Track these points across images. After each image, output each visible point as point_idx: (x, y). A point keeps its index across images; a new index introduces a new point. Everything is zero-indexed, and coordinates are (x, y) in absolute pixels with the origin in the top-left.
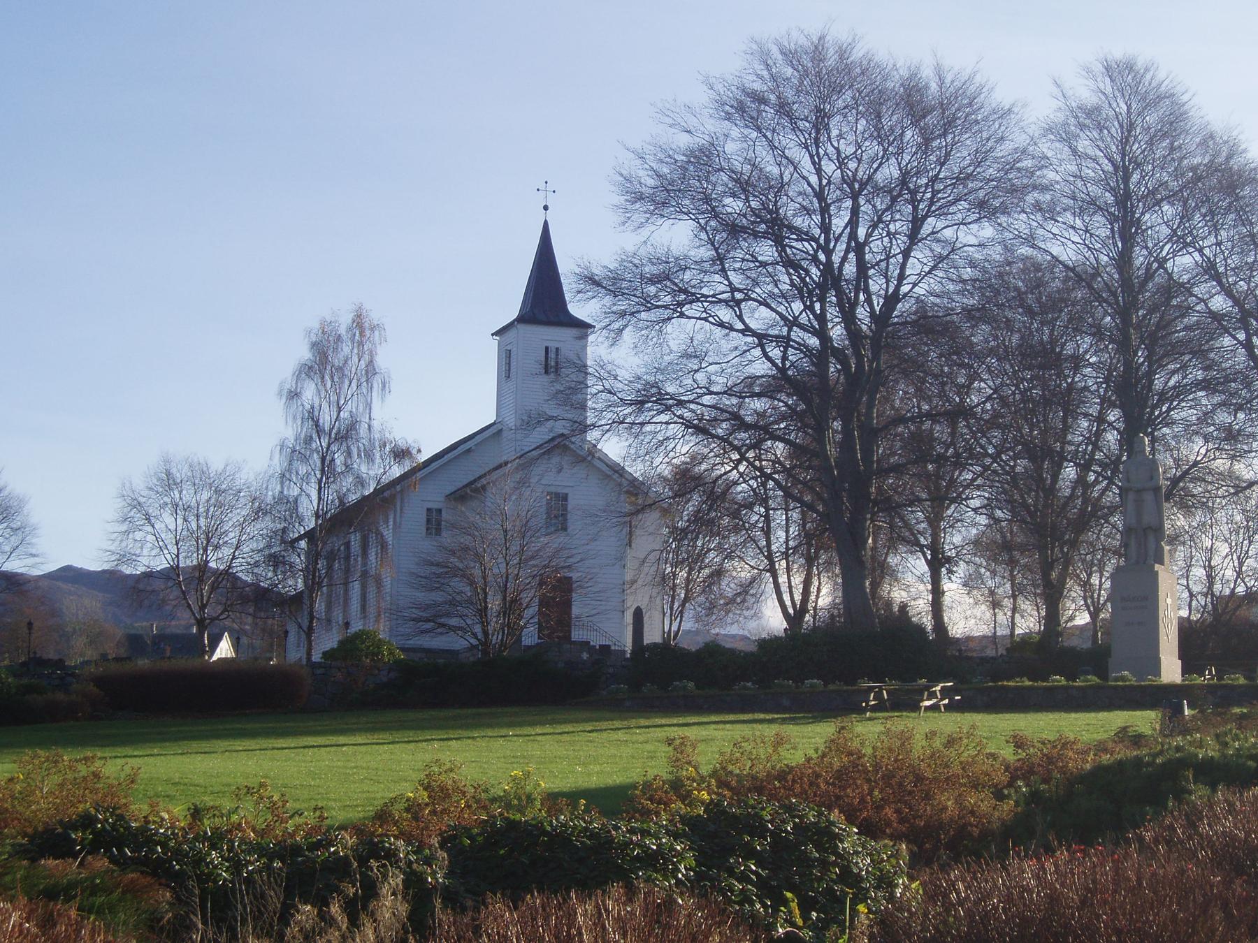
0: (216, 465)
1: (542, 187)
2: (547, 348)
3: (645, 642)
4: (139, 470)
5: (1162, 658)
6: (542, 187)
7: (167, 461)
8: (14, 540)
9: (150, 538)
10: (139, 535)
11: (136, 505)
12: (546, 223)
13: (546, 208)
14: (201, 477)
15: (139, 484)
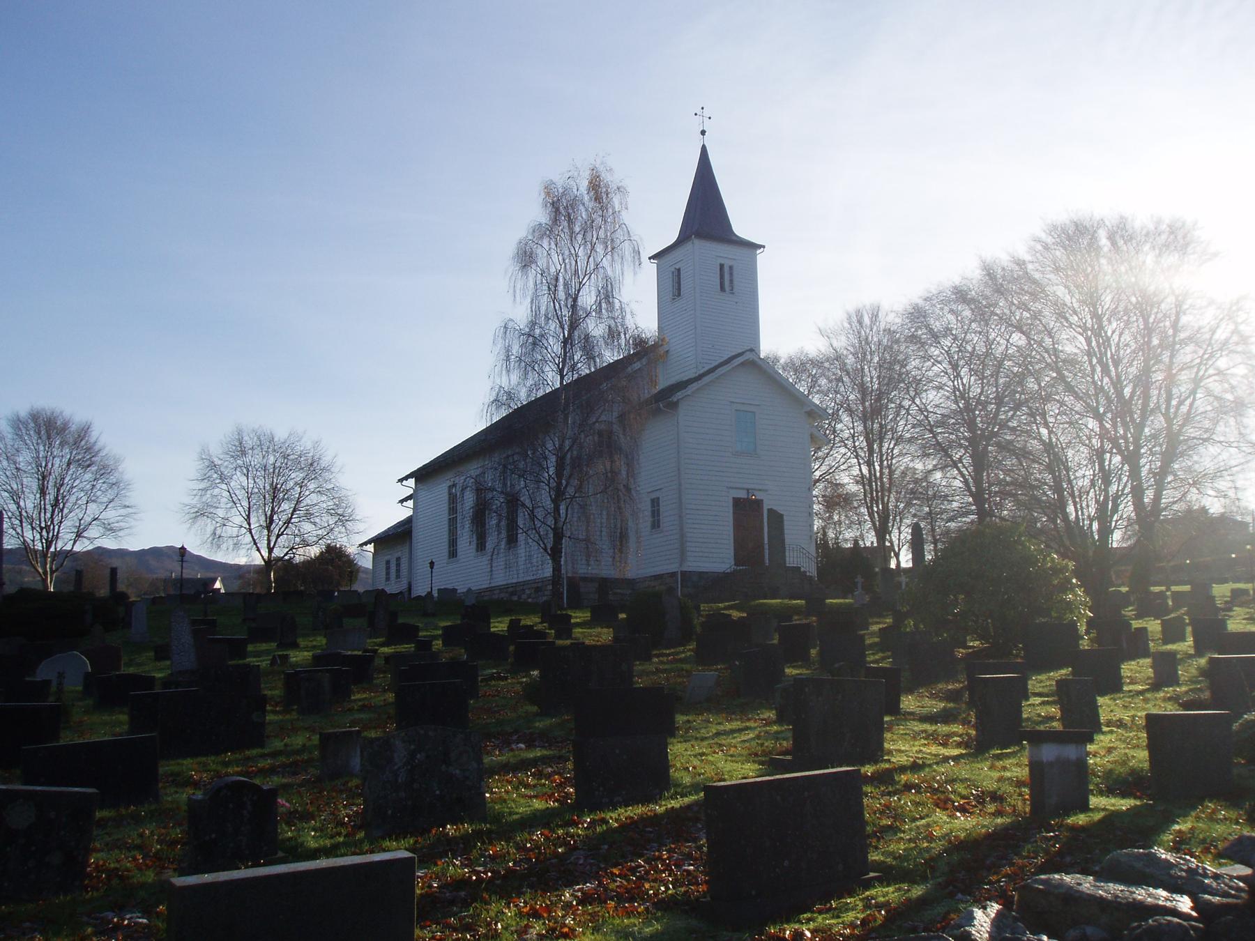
0: (281, 434)
1: (699, 111)
2: (722, 266)
3: (1101, 700)
4: (216, 440)
5: (731, 529)
6: (699, 111)
7: (240, 432)
8: (111, 494)
9: (226, 494)
10: (216, 491)
11: (213, 466)
12: (704, 149)
13: (703, 133)
14: (266, 443)
15: (216, 452)
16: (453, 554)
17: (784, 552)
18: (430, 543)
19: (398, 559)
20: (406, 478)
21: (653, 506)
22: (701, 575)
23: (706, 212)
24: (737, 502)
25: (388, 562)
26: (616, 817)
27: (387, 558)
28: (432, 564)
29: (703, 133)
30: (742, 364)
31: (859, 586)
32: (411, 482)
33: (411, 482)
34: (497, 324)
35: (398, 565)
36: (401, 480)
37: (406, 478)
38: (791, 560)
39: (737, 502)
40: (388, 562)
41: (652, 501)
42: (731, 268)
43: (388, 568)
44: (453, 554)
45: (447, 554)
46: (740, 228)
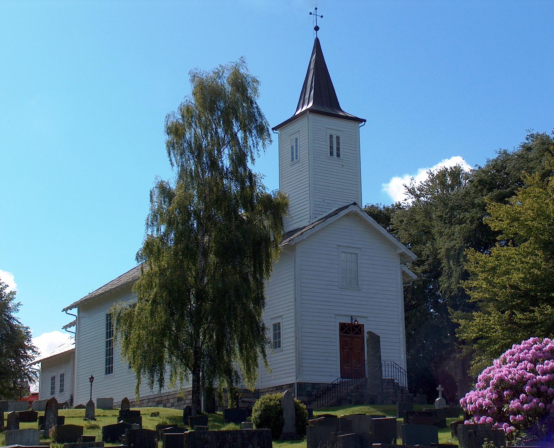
1: (313, 11)
2: (331, 136)
6: (313, 11)
12: (317, 41)
16: (109, 370)
17: (381, 367)
18: (82, 369)
19: (62, 376)
20: (70, 308)
21: (275, 330)
22: (314, 385)
23: (321, 91)
24: (343, 327)
25: (53, 378)
26: (217, 424)
27: (53, 374)
28: (92, 379)
29: (317, 28)
30: (347, 215)
31: (440, 394)
32: (75, 311)
33: (75, 311)
34: (151, 185)
35: (62, 381)
36: (65, 310)
37: (70, 308)
38: (387, 373)
39: (343, 327)
40: (53, 378)
41: (275, 325)
42: (338, 138)
43: (53, 384)
44: (109, 370)
45: (104, 370)
46: (347, 105)
